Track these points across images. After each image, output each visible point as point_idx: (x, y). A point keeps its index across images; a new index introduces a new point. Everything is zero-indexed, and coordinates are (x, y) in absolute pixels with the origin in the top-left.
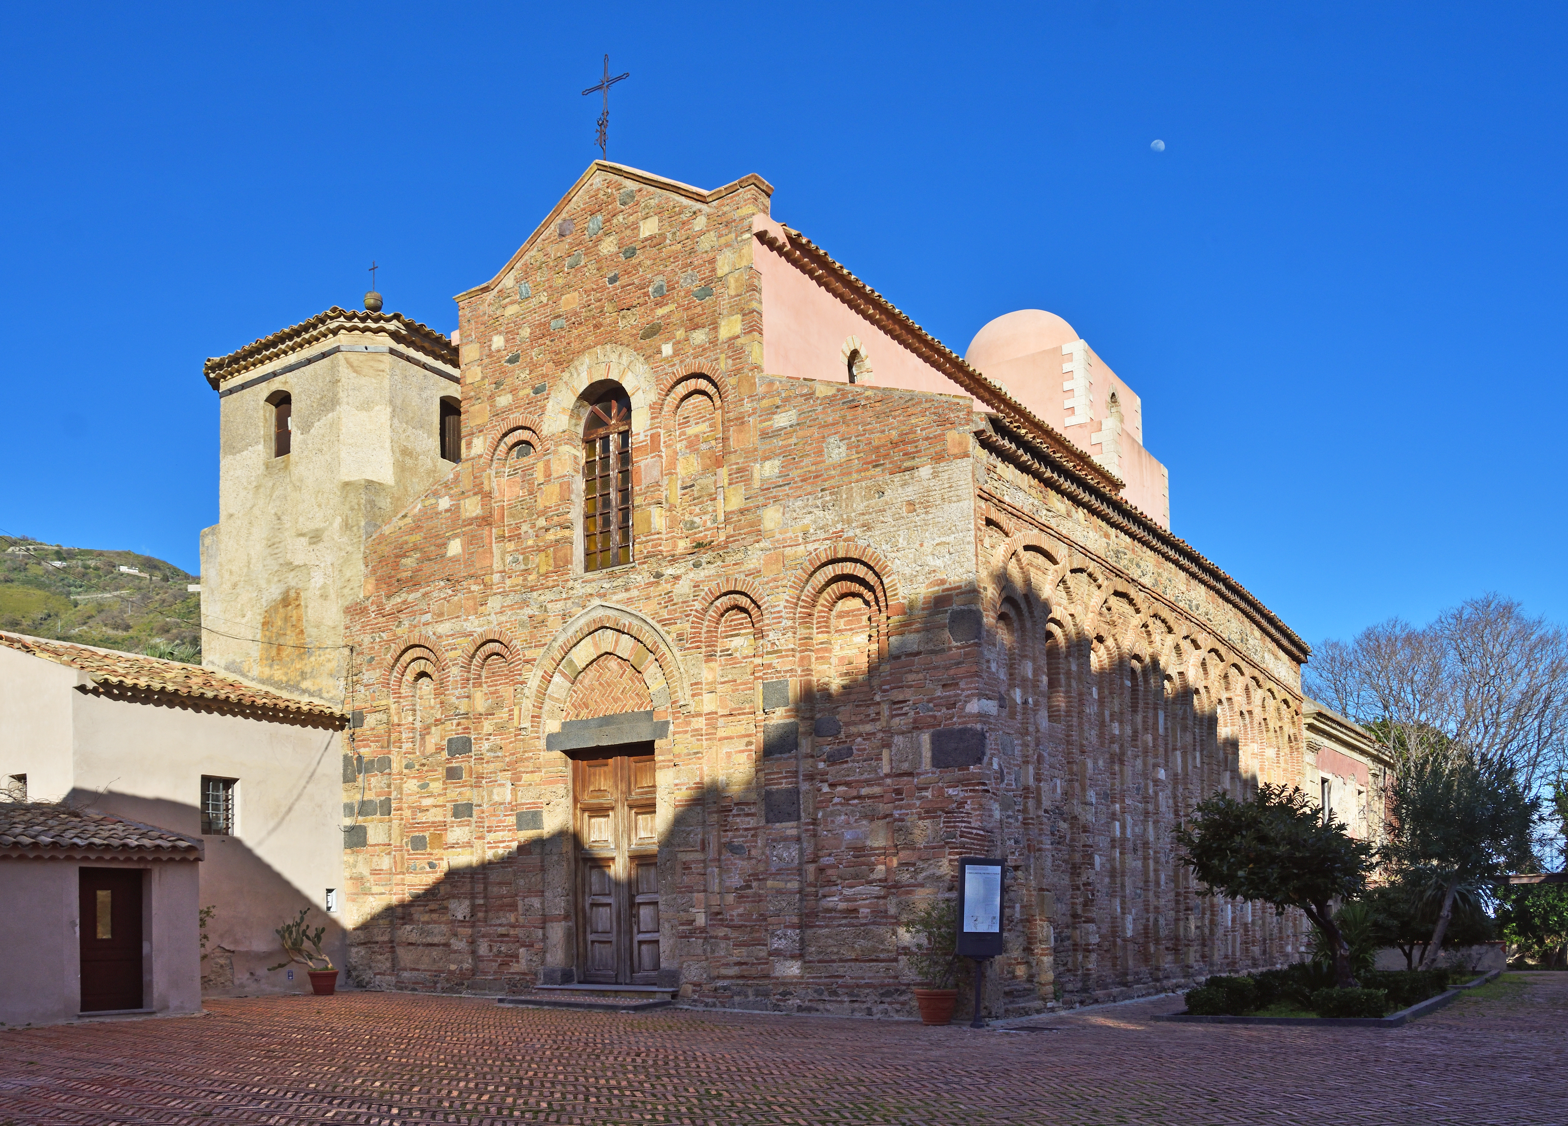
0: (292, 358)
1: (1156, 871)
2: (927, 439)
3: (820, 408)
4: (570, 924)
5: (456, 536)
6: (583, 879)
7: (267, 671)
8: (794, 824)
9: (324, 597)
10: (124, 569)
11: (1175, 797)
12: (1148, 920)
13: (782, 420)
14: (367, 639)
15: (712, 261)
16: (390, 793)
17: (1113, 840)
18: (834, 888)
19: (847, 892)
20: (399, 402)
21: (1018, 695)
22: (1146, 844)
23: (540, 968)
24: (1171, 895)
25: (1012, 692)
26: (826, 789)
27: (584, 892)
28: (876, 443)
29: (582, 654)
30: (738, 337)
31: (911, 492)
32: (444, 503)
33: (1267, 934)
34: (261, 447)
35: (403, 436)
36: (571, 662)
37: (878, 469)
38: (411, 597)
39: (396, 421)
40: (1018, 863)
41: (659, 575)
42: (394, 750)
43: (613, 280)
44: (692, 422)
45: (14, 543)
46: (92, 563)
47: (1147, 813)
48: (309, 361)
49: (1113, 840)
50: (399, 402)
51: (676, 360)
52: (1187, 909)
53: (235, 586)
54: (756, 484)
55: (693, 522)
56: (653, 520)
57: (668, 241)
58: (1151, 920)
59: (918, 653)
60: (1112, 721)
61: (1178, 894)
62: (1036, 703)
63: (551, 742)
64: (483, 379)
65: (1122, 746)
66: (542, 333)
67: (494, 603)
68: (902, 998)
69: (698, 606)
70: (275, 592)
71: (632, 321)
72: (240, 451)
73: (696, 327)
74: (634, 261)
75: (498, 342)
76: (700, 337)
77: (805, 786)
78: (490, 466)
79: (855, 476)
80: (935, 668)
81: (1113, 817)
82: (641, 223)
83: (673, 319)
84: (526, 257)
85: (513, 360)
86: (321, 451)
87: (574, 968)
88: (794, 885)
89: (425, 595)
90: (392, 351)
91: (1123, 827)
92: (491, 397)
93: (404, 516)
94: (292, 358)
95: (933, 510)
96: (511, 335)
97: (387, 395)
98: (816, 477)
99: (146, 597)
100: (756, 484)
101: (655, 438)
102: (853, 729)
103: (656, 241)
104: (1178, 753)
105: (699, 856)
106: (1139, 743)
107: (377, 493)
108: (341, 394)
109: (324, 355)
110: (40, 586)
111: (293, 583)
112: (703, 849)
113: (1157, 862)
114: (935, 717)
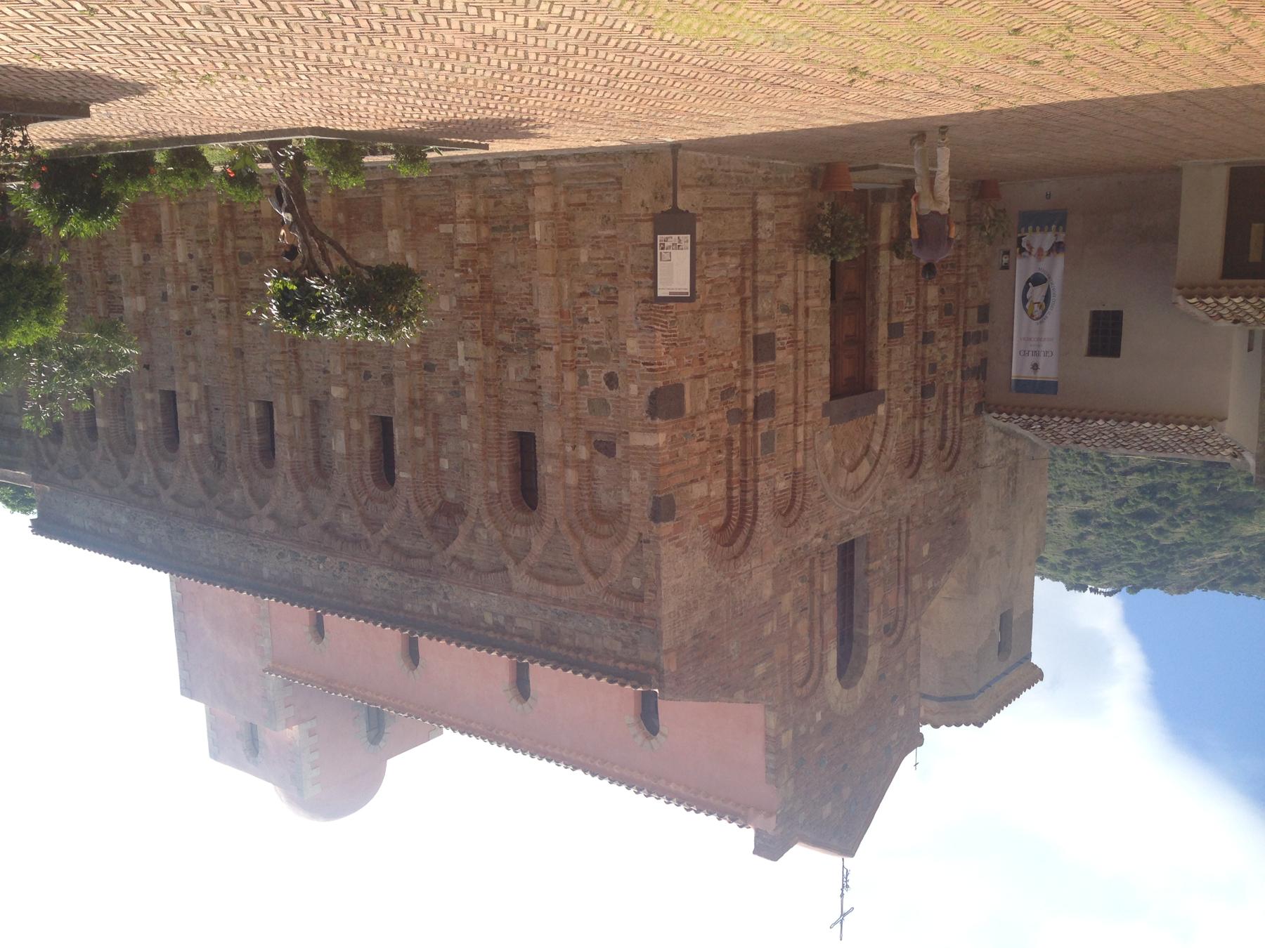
8: (760, 332)
19: (723, 272)
21: (583, 453)
26: (735, 364)
29: (865, 467)
32: (930, 584)
40: (582, 300)
59: (692, 481)
63: (881, 397)
68: (699, 174)
69: (806, 513)
77: (750, 365)
87: (870, 203)
88: (760, 278)
102: (720, 416)
105: (810, 303)
112: (807, 310)
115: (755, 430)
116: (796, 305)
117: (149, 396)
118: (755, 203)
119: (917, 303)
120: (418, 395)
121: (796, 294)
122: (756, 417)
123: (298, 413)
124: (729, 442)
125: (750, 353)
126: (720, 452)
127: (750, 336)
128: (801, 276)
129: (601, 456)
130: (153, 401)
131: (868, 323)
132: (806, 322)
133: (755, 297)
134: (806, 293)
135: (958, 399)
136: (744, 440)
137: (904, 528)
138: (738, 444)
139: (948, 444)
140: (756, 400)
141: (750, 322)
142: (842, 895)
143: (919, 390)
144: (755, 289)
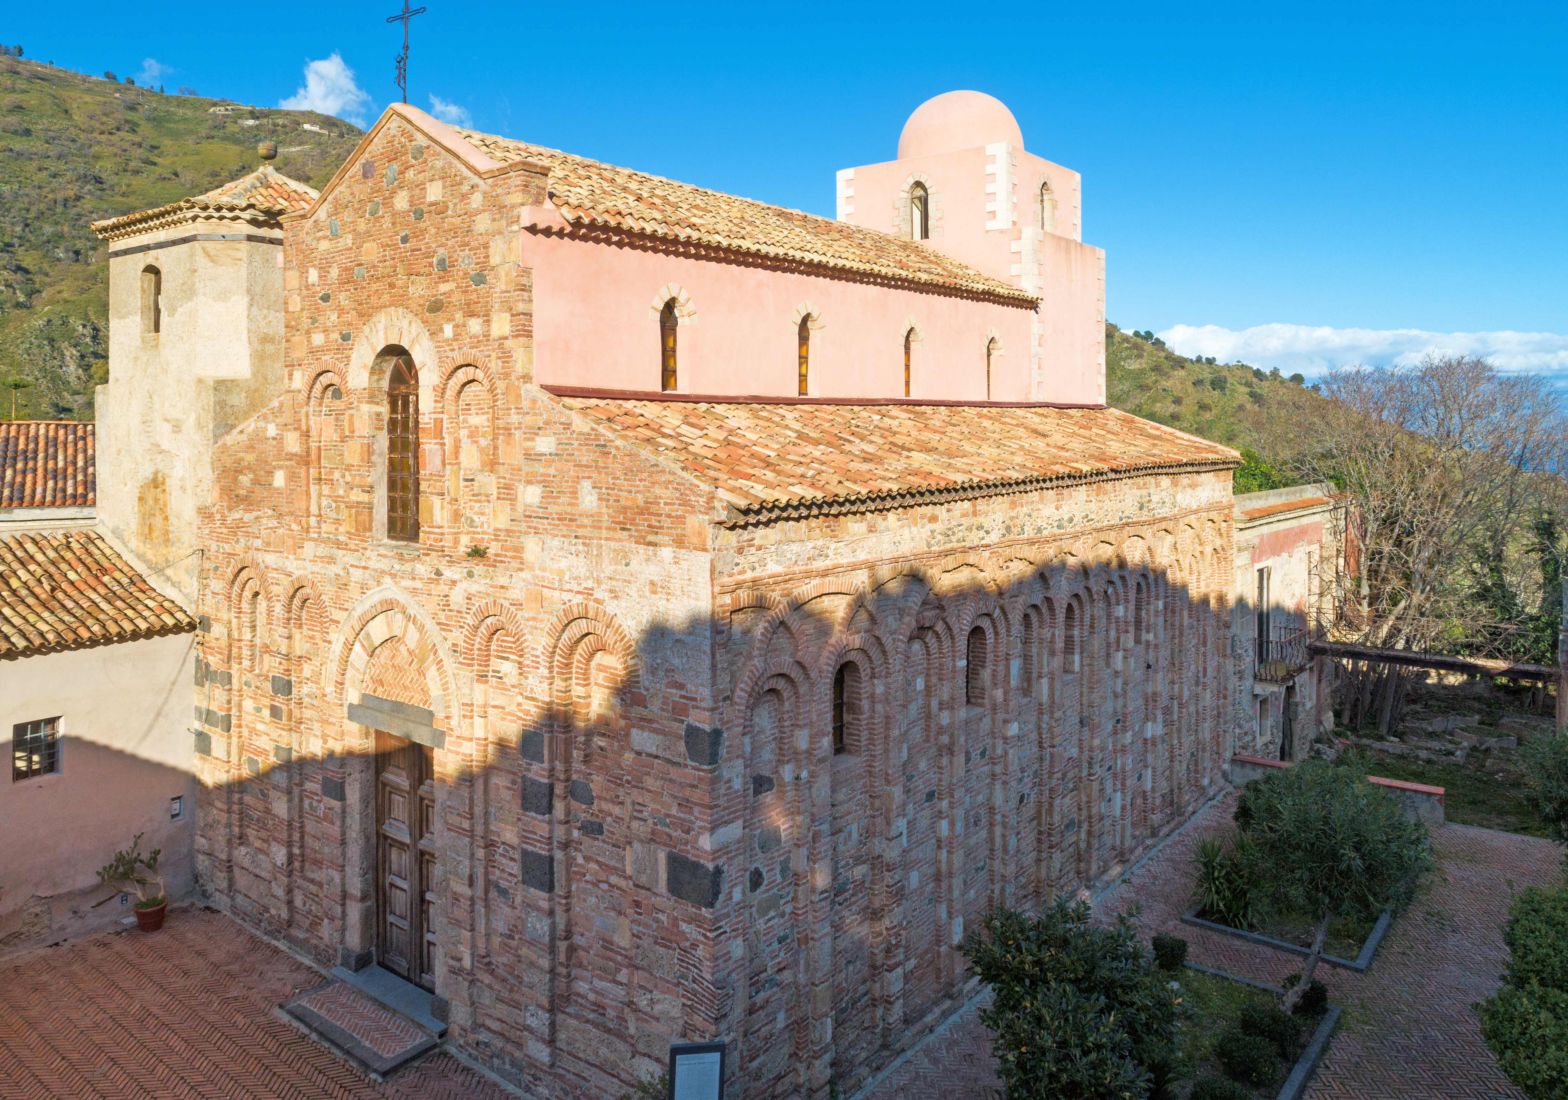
0: (162, 235)
1: (1004, 836)
2: (669, 516)
3: (576, 443)
4: (369, 903)
5: (281, 468)
6: (384, 856)
7: (142, 548)
9: (183, 489)
10: (307, 127)
11: (1039, 728)
12: (993, 891)
13: (545, 444)
14: (214, 547)
15: (486, 246)
16: (229, 709)
17: (939, 841)
18: (585, 973)
20: (258, 289)
22: (992, 810)
23: (339, 947)
24: (1033, 836)
25: (780, 769)
27: (384, 870)
28: (623, 502)
30: (506, 338)
31: (652, 572)
33: (1175, 784)
34: (138, 318)
35: (263, 323)
36: (368, 635)
37: (626, 533)
38: (248, 517)
39: (255, 309)
41: (439, 573)
42: (235, 666)
43: (405, 240)
44: (473, 411)
45: (215, 105)
46: (280, 122)
47: (994, 776)
48: (174, 243)
49: (939, 841)
50: (258, 289)
51: (455, 345)
52: (1051, 847)
53: (119, 452)
54: (520, 509)
55: (472, 521)
56: (436, 512)
57: (450, 212)
58: (997, 892)
60: (940, 709)
61: (1040, 833)
62: (812, 775)
64: (302, 309)
65: (952, 736)
66: (348, 279)
67: (309, 549)
70: (146, 472)
71: (418, 289)
72: (123, 317)
73: (472, 315)
74: (422, 225)
75: (313, 275)
76: (475, 326)
77: (559, 855)
78: (307, 404)
79: (604, 533)
80: (671, 780)
81: (940, 815)
82: (428, 185)
83: (453, 299)
84: (336, 192)
85: (326, 298)
86: (182, 338)
87: (373, 949)
89: (257, 518)
90: (250, 238)
91: (952, 824)
92: (308, 332)
93: (242, 432)
94: (162, 235)
95: (673, 600)
96: (324, 271)
97: (245, 285)
98: (571, 520)
99: (324, 153)
100: (520, 509)
101: (439, 423)
103: (440, 209)
104: (1045, 681)
106: (986, 701)
107: (229, 391)
108: (198, 285)
109: (185, 240)
110: (236, 141)
111: (160, 467)
113: (1004, 825)
114: (669, 836)
115: (552, 770)
116: (487, 891)
117: (1151, 637)
118: (552, 1055)
119: (301, 800)
120: (945, 761)
121: (487, 907)
122: (551, 787)
123: (1045, 681)
124: (587, 759)
125: (559, 869)
126: (601, 748)
127: (559, 891)
128: (481, 927)
129: (766, 773)
130: (1148, 632)
131: (373, 803)
132: (472, 868)
133: (553, 939)
134: (472, 905)
135: (235, 650)
136: (567, 760)
137: (313, 521)
138: (575, 753)
139: (248, 594)
140: (550, 808)
141: (559, 910)
142: (406, 48)
143: (294, 690)
144: (552, 950)
